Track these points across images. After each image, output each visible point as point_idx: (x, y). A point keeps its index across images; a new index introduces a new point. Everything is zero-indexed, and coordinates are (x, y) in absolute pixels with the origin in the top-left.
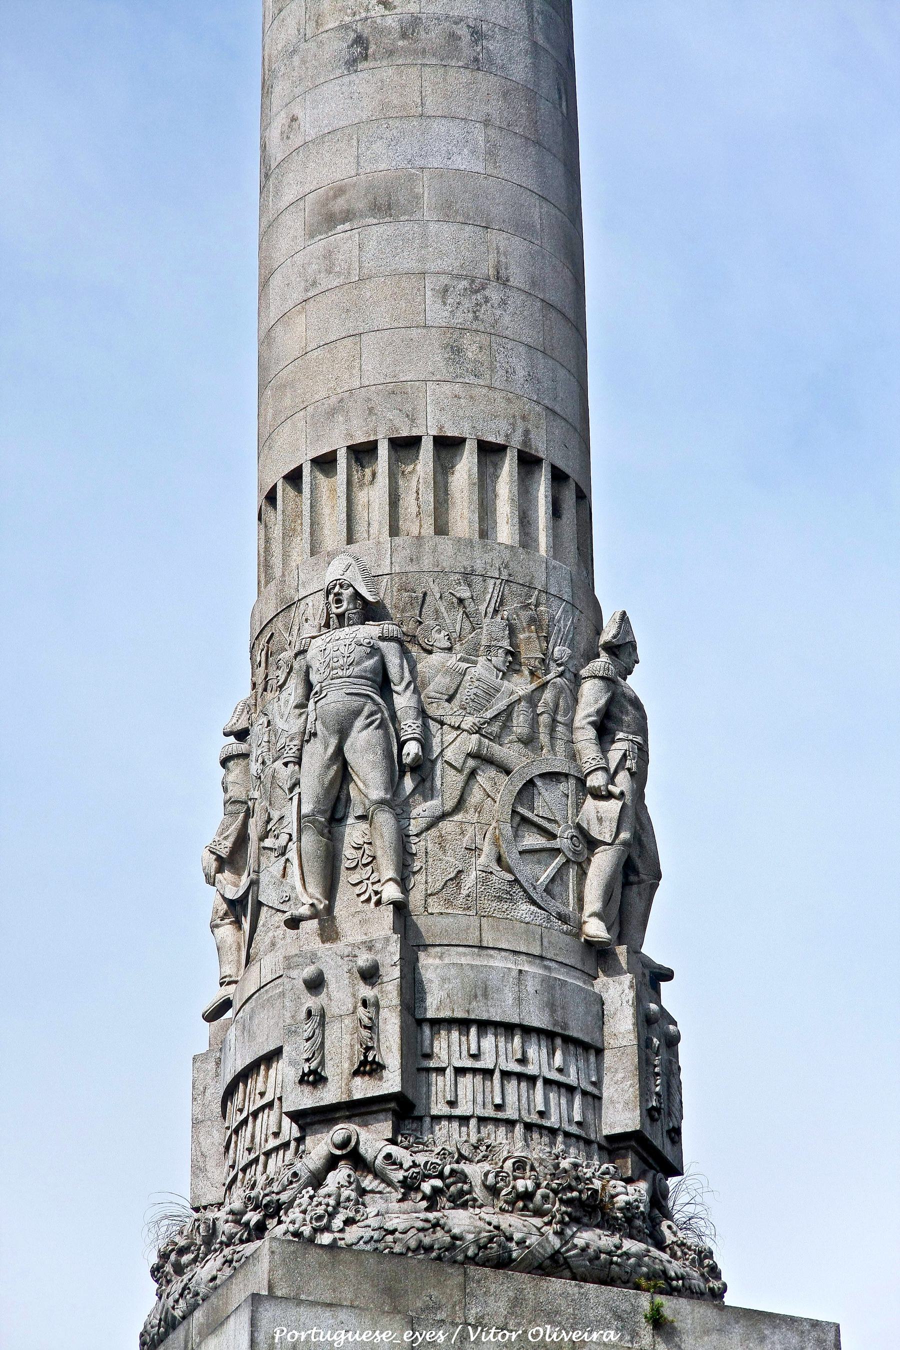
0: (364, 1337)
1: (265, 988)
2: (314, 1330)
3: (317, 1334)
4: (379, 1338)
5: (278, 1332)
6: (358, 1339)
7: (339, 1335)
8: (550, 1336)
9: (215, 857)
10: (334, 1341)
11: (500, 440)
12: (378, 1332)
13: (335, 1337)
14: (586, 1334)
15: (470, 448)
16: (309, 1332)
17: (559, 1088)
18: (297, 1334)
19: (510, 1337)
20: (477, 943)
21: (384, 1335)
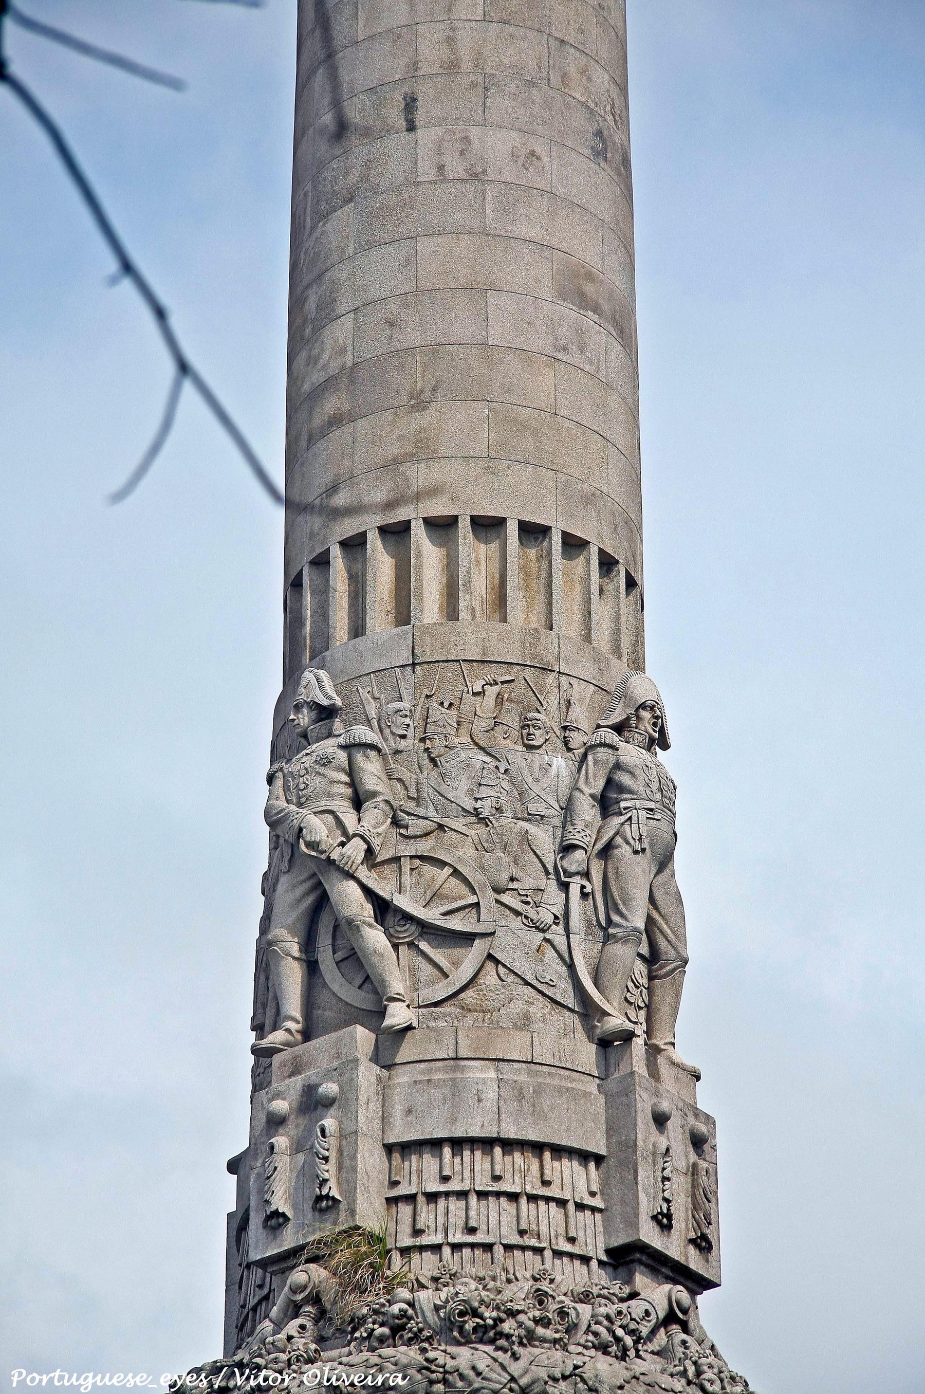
0: (115, 1381)
1: (538, 1067)
2: (58, 1373)
3: (61, 1378)
4: (132, 1382)
5: (16, 1374)
6: (108, 1384)
7: (87, 1378)
8: (328, 1380)
9: (365, 847)
10: (81, 1385)
11: (624, 716)
12: (131, 1375)
13: (81, 1381)
14: (370, 1378)
15: (374, 541)
16: (52, 1375)
17: (593, 1213)
18: (38, 1377)
19: (41, 1380)
20: (452, 1054)
21: (138, 1379)
